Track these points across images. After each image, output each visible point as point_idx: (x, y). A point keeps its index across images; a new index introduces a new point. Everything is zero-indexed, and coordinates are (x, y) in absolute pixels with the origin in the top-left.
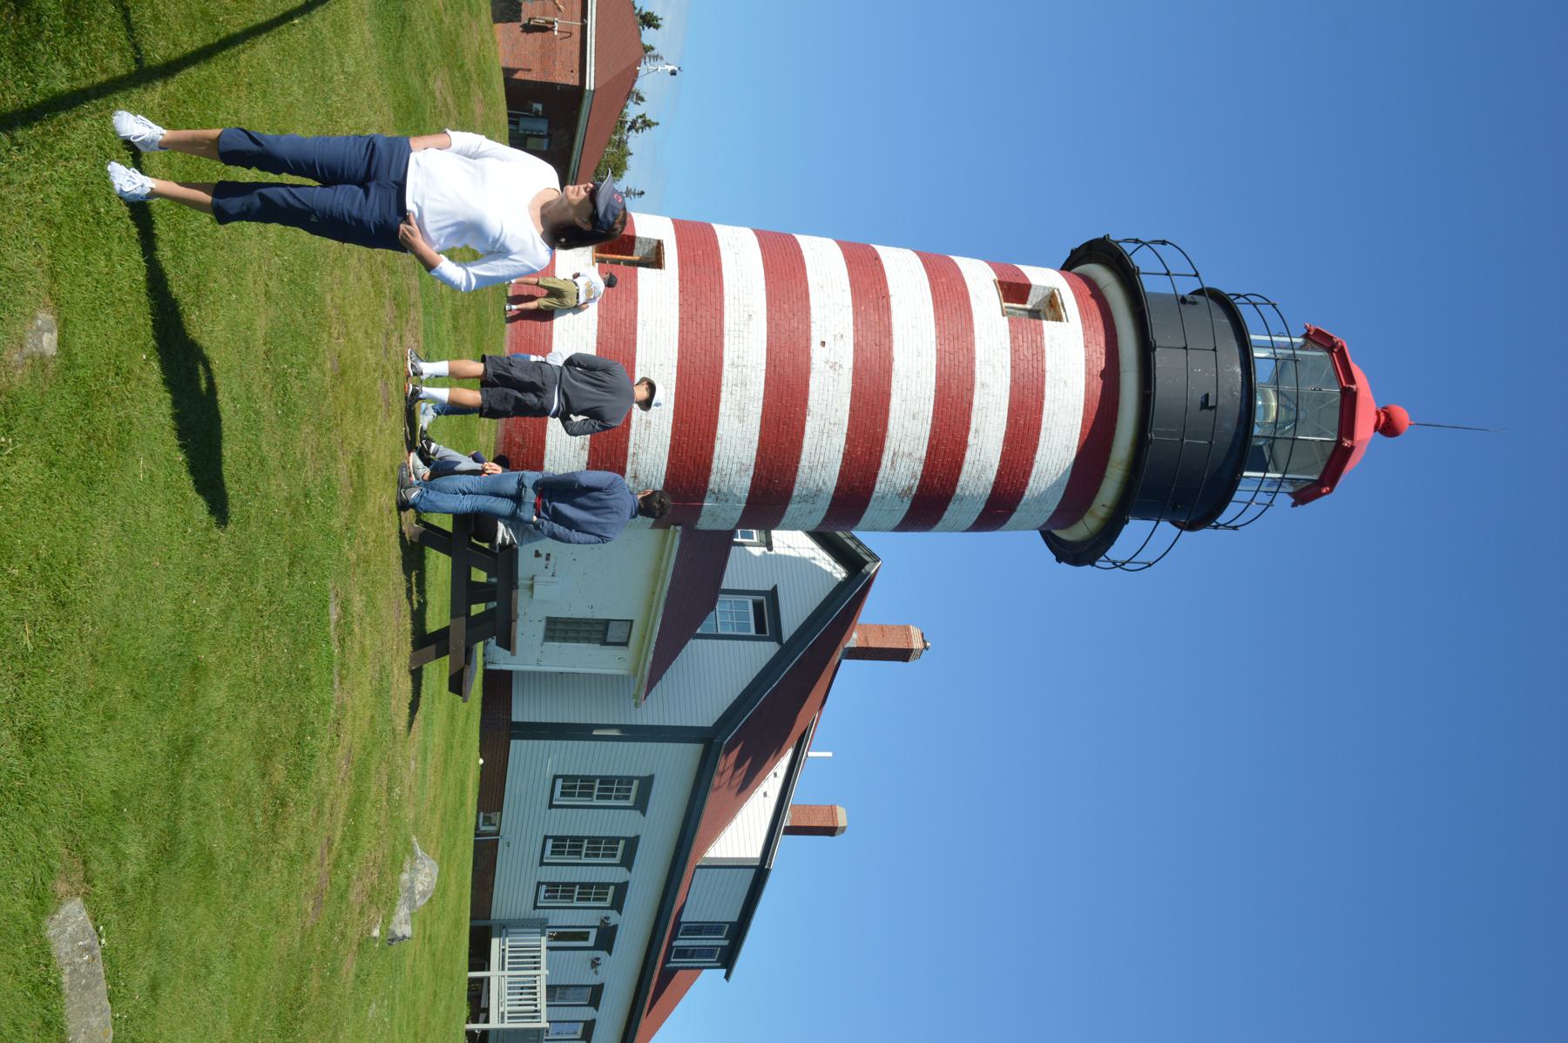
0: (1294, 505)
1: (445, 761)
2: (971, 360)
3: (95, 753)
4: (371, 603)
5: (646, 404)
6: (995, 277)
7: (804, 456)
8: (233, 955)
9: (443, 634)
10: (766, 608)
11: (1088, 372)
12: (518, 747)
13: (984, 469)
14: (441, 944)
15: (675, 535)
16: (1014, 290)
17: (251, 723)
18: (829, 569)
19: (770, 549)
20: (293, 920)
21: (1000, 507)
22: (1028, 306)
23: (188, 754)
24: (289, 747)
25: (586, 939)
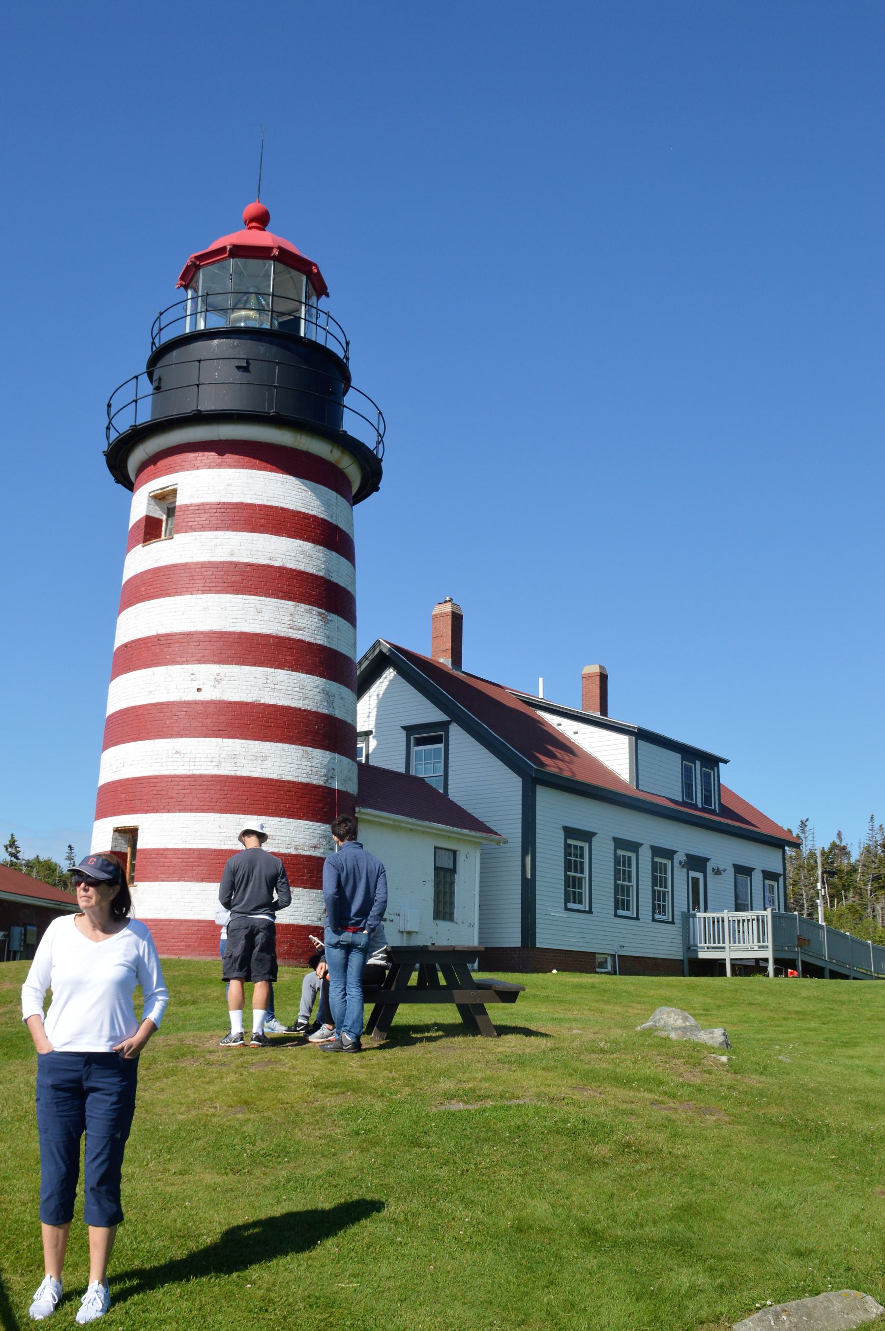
0: (327, 295)
1: (560, 1002)
2: (211, 564)
3: (604, 1318)
4: (445, 1073)
5: (262, 837)
6: (140, 546)
7: (295, 705)
8: (762, 1185)
9: (463, 1009)
10: (421, 735)
11: (219, 466)
12: (542, 942)
13: (303, 552)
14: (709, 1001)
15: (363, 812)
16: (151, 530)
17: (561, 1177)
18: (386, 683)
19: (370, 732)
20: (725, 1132)
21: (333, 538)
22: (164, 517)
23: (596, 1233)
24: (580, 1142)
25: (698, 879)
